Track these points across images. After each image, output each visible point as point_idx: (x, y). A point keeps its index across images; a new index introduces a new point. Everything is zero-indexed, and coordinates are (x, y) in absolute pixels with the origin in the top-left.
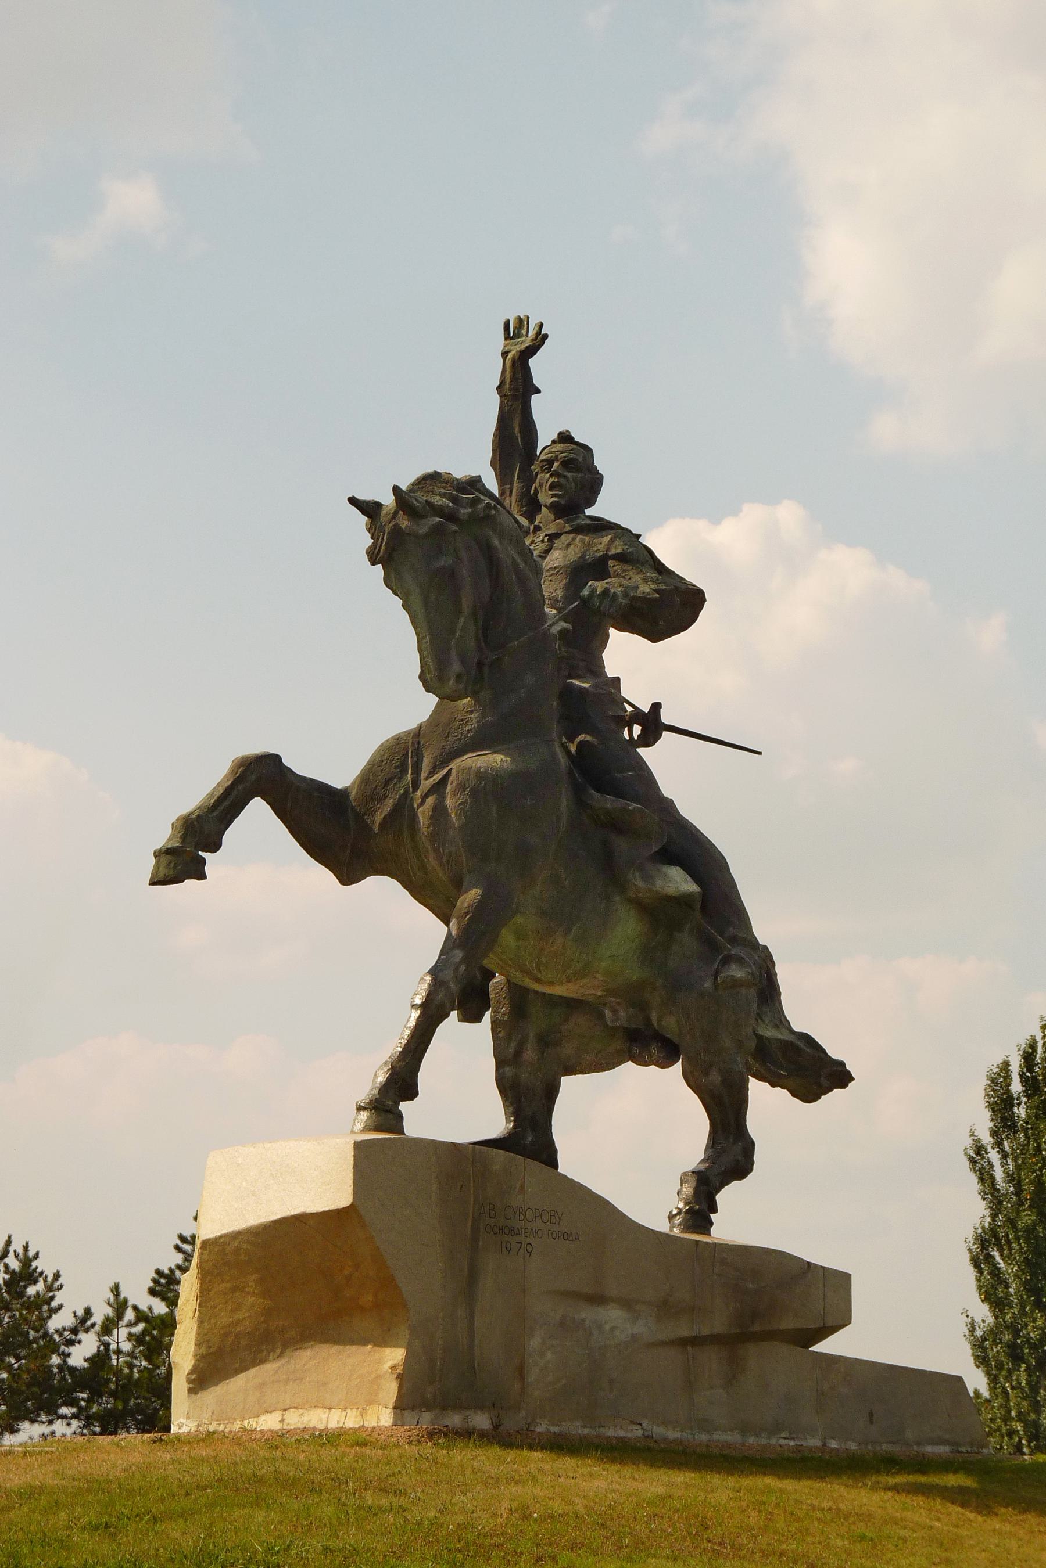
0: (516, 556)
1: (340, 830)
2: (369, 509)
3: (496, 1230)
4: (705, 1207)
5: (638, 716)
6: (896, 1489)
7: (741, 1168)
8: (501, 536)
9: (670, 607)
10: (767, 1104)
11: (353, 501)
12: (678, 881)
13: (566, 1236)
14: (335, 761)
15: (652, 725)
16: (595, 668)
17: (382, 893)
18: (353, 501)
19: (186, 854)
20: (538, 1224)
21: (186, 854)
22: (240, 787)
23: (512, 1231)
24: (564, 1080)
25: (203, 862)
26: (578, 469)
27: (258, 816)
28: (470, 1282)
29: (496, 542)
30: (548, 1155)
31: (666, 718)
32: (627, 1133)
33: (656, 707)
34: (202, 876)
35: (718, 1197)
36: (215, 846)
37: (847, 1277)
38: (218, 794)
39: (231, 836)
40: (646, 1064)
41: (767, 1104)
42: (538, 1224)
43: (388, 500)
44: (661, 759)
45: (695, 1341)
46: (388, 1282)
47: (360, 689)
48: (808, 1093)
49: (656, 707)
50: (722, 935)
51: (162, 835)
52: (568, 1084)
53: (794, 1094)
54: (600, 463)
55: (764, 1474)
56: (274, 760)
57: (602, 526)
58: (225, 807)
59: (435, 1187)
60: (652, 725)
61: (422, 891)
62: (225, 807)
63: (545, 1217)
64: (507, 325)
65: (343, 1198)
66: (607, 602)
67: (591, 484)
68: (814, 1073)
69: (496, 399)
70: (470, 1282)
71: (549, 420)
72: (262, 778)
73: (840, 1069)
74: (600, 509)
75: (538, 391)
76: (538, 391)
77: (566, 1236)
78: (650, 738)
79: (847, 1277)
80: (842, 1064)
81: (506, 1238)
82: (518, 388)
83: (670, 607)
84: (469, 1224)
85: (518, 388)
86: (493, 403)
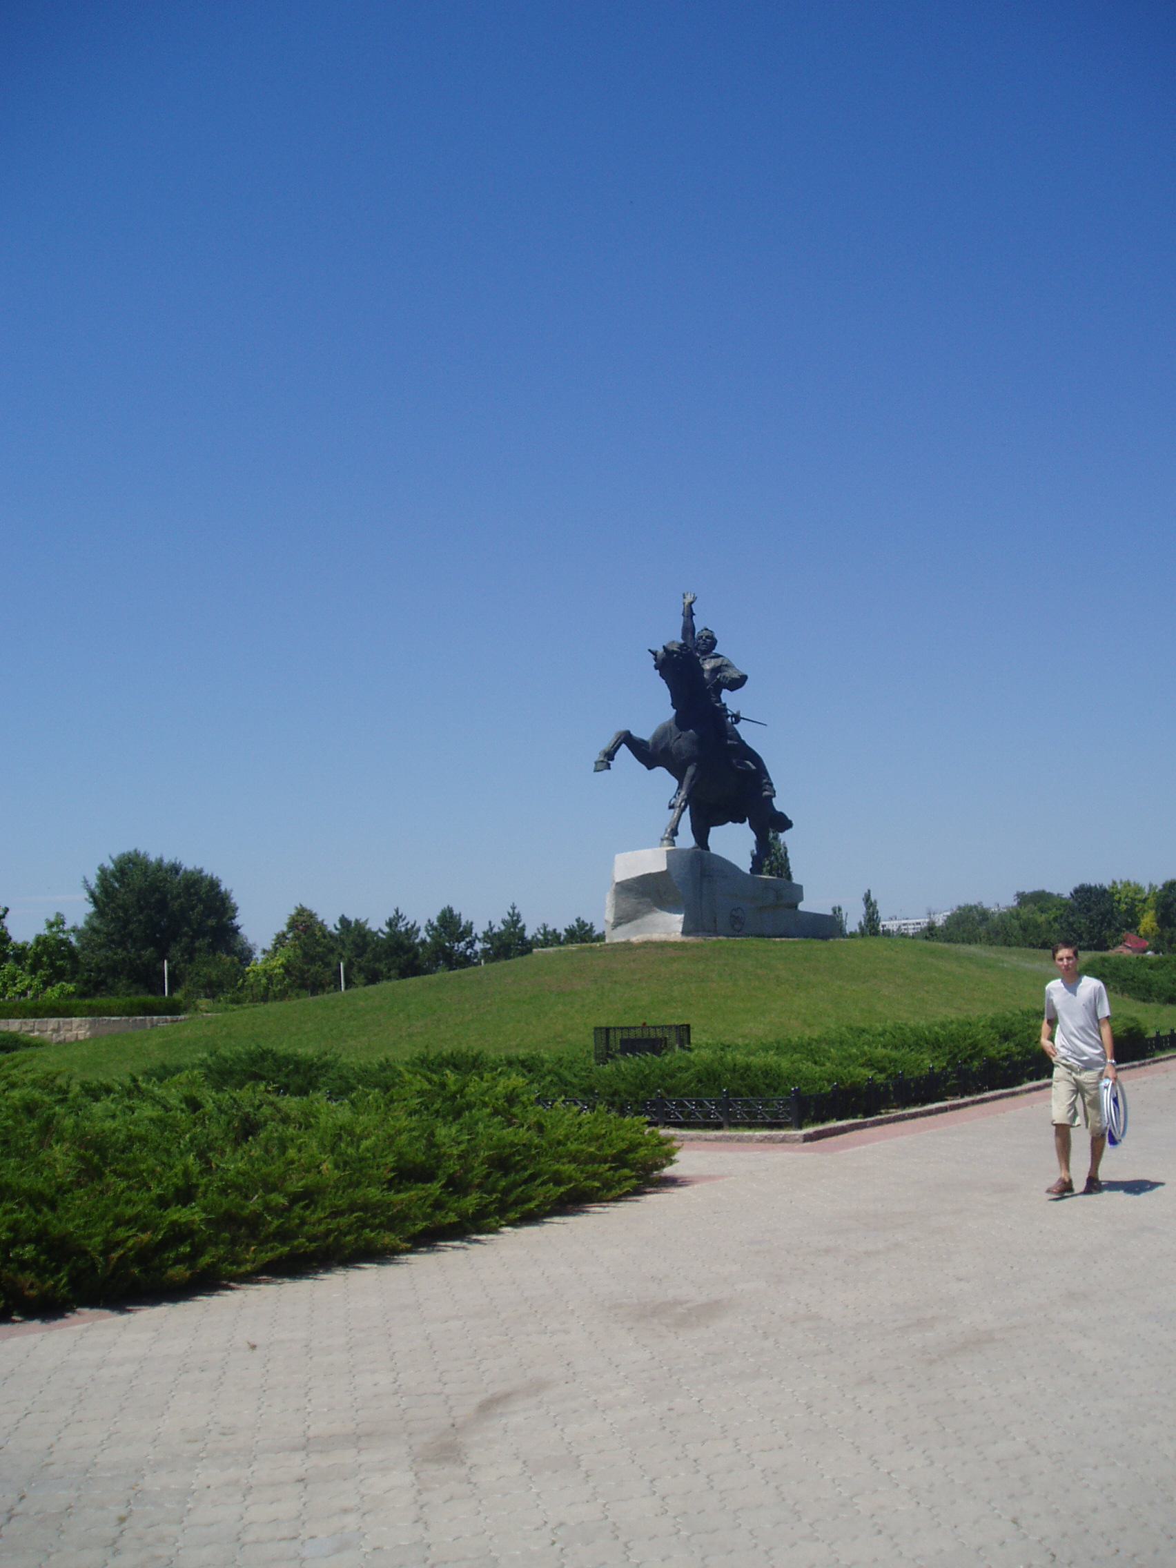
1: (648, 754)
5: (733, 716)
6: (808, 1138)
9: (738, 683)
11: (1162, 1184)
14: (645, 732)
15: (737, 718)
16: (719, 700)
17: (661, 772)
18: (1162, 1184)
30: (708, 849)
32: (734, 843)
43: (661, 651)
44: (741, 728)
47: (653, 709)
51: (597, 756)
52: (713, 829)
57: (718, 656)
60: (737, 718)
61: (672, 771)
62: (616, 748)
65: (664, 868)
67: (714, 643)
72: (627, 739)
82: (689, 614)
85: (689, 614)
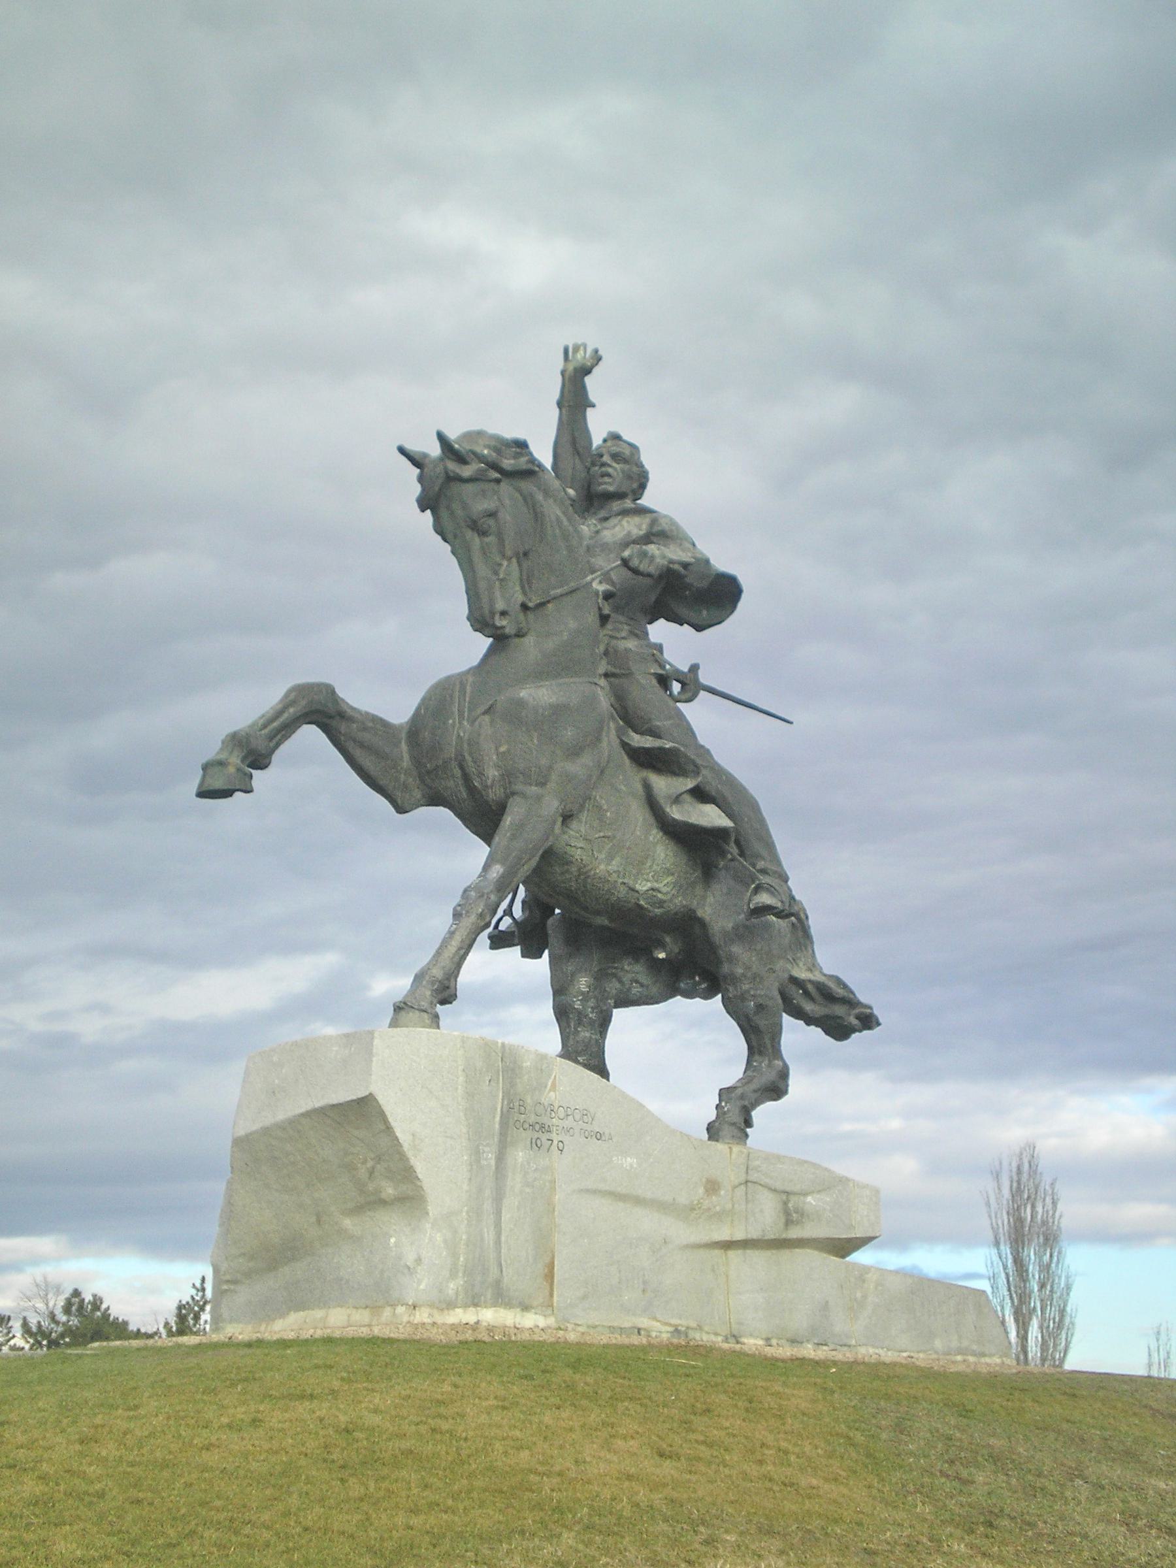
0: (560, 514)
2: (416, 460)
3: (526, 1126)
7: (776, 1090)
8: (547, 493)
10: (797, 1037)
11: (402, 451)
13: (599, 1136)
18: (402, 451)
20: (569, 1122)
22: (291, 710)
24: (615, 1011)
26: (626, 461)
27: (310, 736)
29: (540, 497)
31: (704, 678)
33: (694, 668)
35: (753, 1113)
38: (269, 715)
41: (797, 1037)
42: (569, 1122)
43: (434, 450)
45: (728, 1245)
46: (407, 1174)
49: (694, 668)
50: (754, 866)
52: (620, 1015)
54: (646, 459)
55: (894, 1364)
58: (281, 727)
59: (461, 1079)
60: (691, 685)
63: (578, 1117)
66: (646, 561)
67: (640, 481)
69: (555, 412)
71: (598, 426)
72: (321, 710)
73: (869, 1011)
74: (646, 501)
75: (594, 406)
76: (594, 406)
77: (599, 1136)
81: (536, 1135)
82: (574, 400)
83: (707, 596)
84: (498, 1119)
85: (574, 400)
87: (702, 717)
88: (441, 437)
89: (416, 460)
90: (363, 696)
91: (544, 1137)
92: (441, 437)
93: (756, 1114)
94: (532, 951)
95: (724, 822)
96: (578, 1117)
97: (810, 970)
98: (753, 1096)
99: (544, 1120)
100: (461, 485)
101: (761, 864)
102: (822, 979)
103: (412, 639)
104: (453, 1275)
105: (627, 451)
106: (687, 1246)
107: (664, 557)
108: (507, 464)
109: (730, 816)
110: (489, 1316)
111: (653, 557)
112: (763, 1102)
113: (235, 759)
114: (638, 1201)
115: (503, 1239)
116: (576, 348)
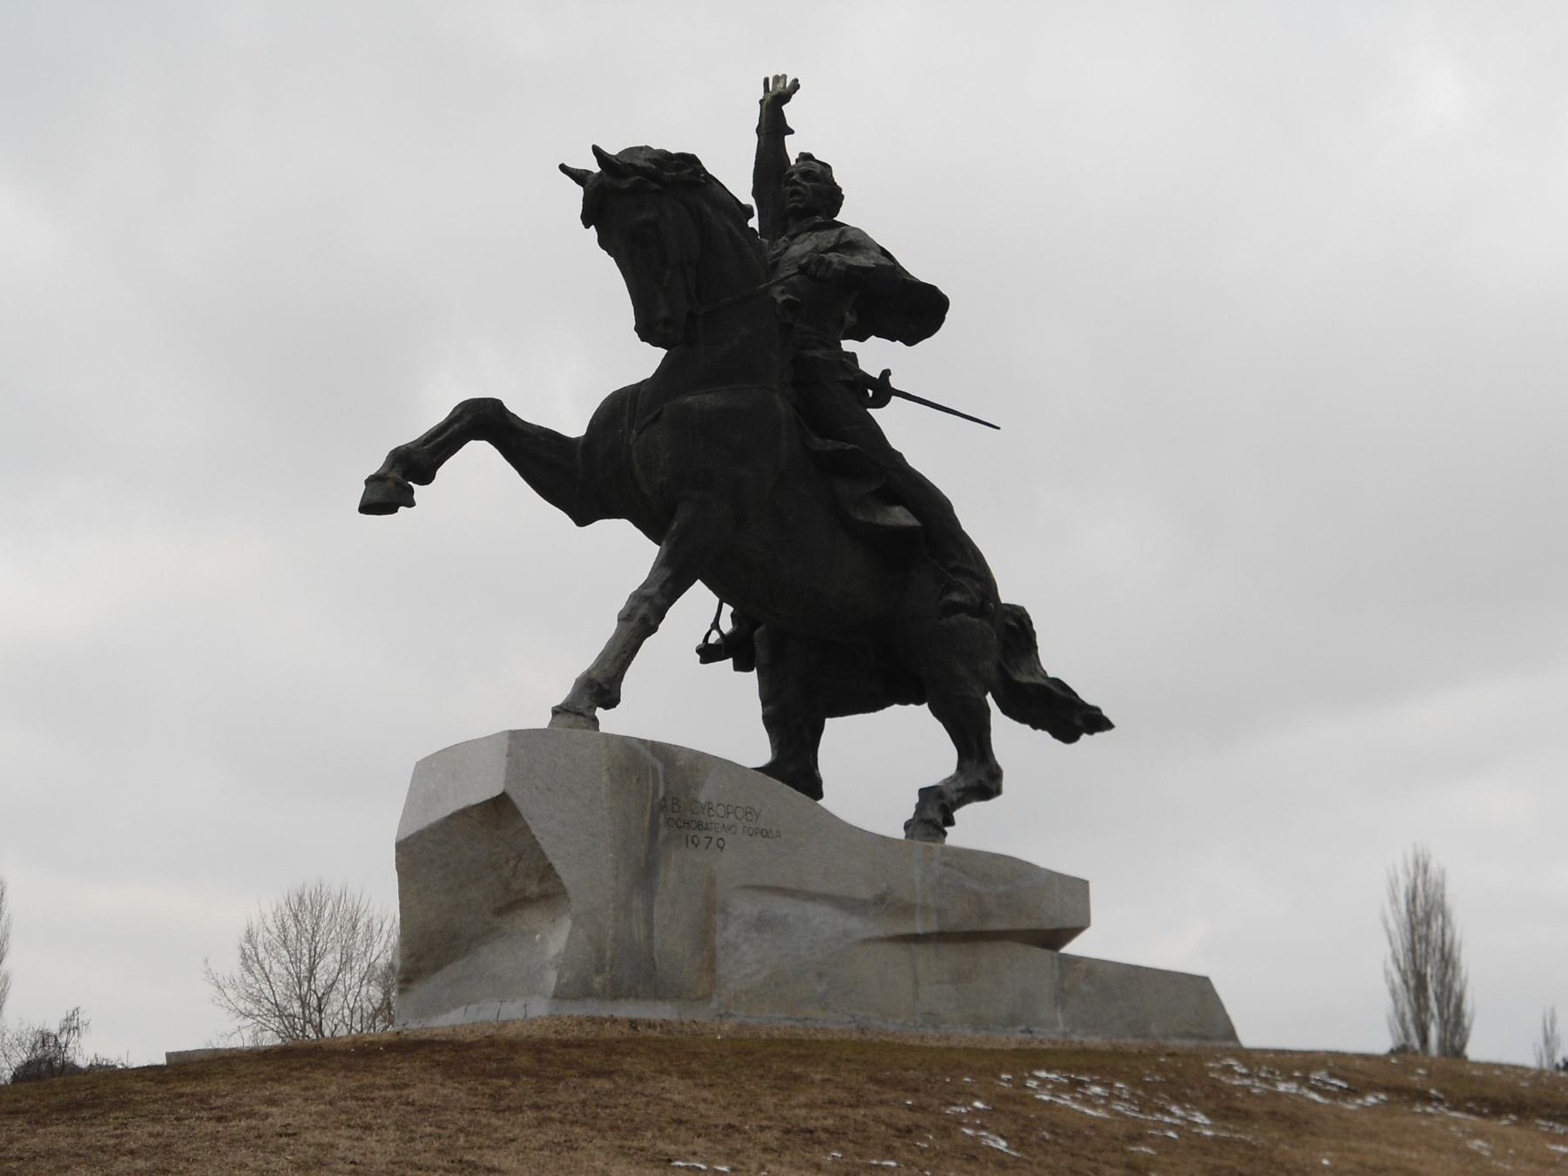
1: (572, 474)
2: (578, 176)
4: (940, 820)
10: (1011, 739)
11: (563, 168)
12: (900, 516)
18: (563, 168)
19: (397, 482)
21: (397, 482)
22: (456, 426)
23: (699, 826)
24: (828, 721)
25: (412, 491)
27: (479, 456)
28: (645, 874)
30: (812, 787)
31: (895, 382)
33: (886, 374)
34: (411, 504)
36: (426, 478)
37: (1086, 883)
39: (447, 471)
40: (998, 767)
41: (1011, 739)
45: (915, 938)
46: (547, 872)
48: (1067, 734)
49: (886, 374)
53: (1055, 736)
54: (839, 178)
56: (496, 405)
59: (605, 778)
60: (883, 390)
63: (740, 815)
64: (766, 81)
67: (834, 198)
68: (1067, 716)
69: (755, 139)
70: (645, 874)
71: (793, 148)
72: (483, 420)
75: (792, 132)
76: (792, 132)
77: (765, 834)
78: (881, 402)
79: (1086, 883)
80: (1098, 709)
81: (692, 833)
82: (773, 126)
83: (915, 310)
84: (647, 817)
85: (773, 126)
86: (753, 141)
87: (891, 420)
88: (597, 151)
89: (578, 176)
90: (528, 409)
91: (702, 835)
92: (597, 151)
93: (957, 814)
94: (741, 666)
95: (911, 521)
96: (740, 815)
97: (1032, 674)
98: (954, 797)
99: (704, 818)
100: (638, 201)
101: (953, 563)
102: (1044, 682)
103: (582, 349)
104: (599, 970)
105: (818, 169)
106: (866, 941)
107: (843, 263)
108: (679, 176)
109: (917, 515)
110: (627, 1010)
111: (830, 263)
112: (969, 802)
113: (396, 475)
114: (812, 897)
115: (656, 934)
116: (777, 79)
